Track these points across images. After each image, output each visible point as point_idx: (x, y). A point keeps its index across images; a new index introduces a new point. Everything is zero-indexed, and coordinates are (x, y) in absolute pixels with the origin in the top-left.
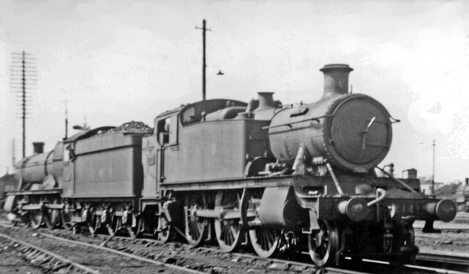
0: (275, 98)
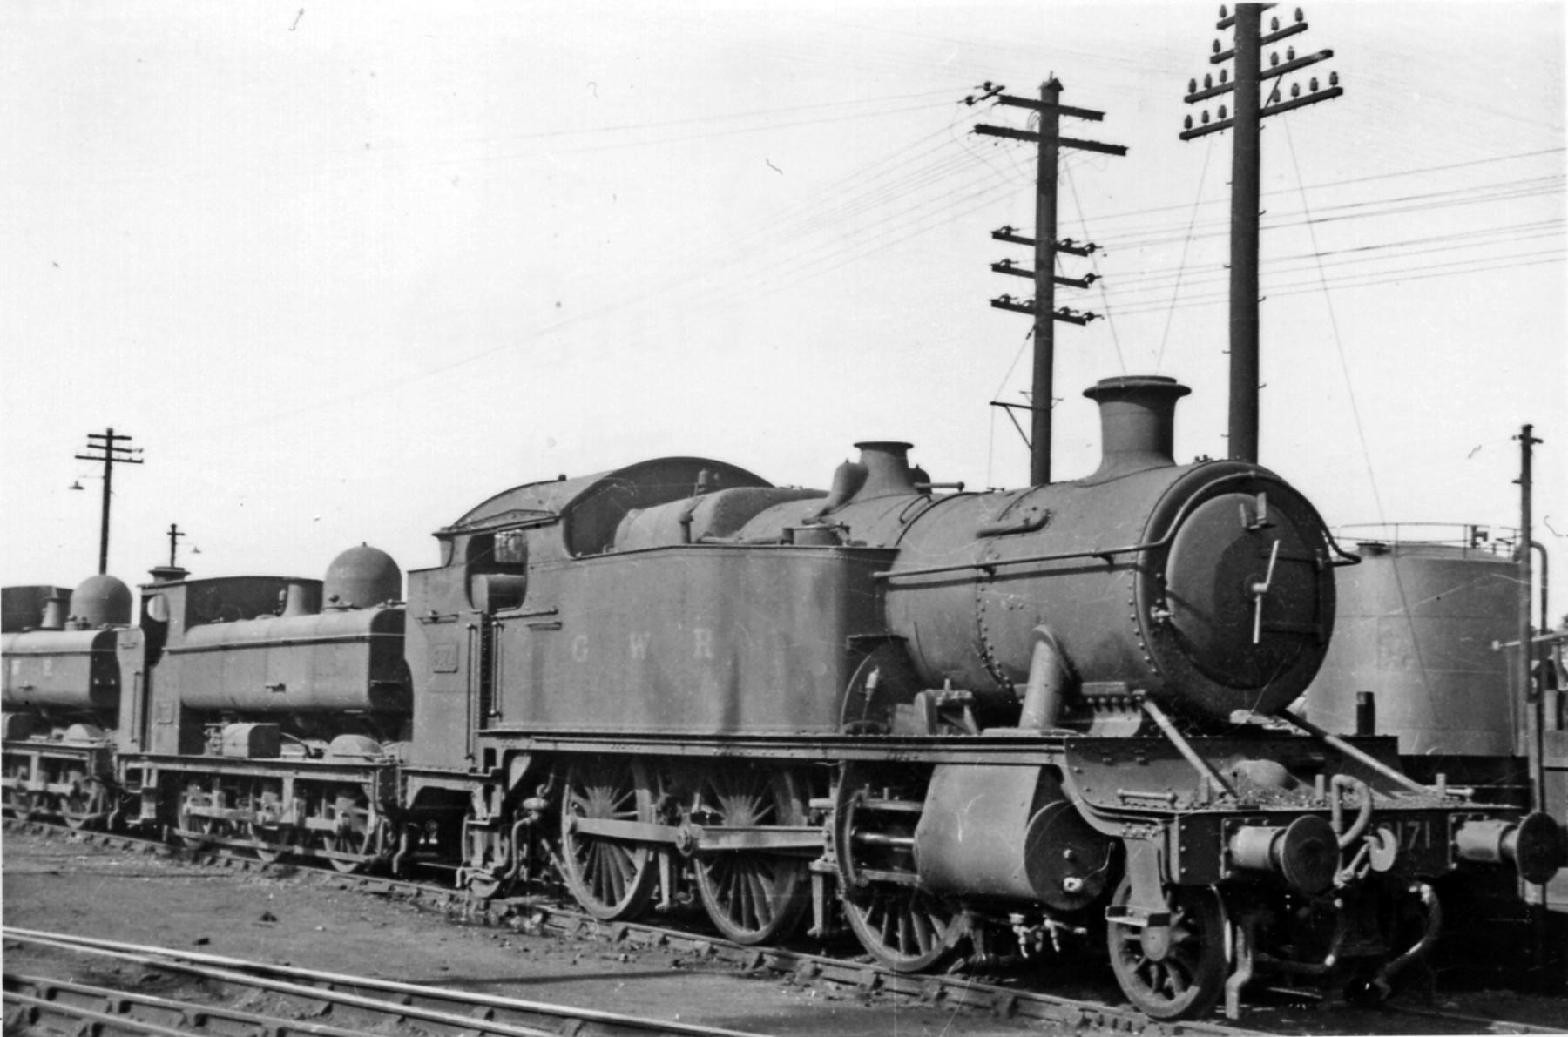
0: (914, 459)
